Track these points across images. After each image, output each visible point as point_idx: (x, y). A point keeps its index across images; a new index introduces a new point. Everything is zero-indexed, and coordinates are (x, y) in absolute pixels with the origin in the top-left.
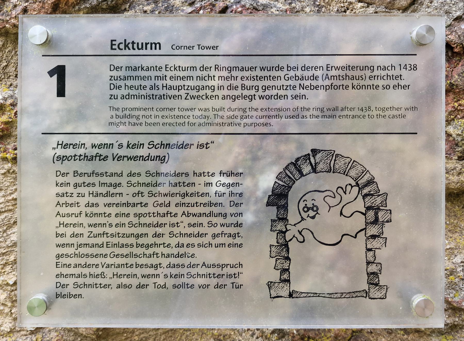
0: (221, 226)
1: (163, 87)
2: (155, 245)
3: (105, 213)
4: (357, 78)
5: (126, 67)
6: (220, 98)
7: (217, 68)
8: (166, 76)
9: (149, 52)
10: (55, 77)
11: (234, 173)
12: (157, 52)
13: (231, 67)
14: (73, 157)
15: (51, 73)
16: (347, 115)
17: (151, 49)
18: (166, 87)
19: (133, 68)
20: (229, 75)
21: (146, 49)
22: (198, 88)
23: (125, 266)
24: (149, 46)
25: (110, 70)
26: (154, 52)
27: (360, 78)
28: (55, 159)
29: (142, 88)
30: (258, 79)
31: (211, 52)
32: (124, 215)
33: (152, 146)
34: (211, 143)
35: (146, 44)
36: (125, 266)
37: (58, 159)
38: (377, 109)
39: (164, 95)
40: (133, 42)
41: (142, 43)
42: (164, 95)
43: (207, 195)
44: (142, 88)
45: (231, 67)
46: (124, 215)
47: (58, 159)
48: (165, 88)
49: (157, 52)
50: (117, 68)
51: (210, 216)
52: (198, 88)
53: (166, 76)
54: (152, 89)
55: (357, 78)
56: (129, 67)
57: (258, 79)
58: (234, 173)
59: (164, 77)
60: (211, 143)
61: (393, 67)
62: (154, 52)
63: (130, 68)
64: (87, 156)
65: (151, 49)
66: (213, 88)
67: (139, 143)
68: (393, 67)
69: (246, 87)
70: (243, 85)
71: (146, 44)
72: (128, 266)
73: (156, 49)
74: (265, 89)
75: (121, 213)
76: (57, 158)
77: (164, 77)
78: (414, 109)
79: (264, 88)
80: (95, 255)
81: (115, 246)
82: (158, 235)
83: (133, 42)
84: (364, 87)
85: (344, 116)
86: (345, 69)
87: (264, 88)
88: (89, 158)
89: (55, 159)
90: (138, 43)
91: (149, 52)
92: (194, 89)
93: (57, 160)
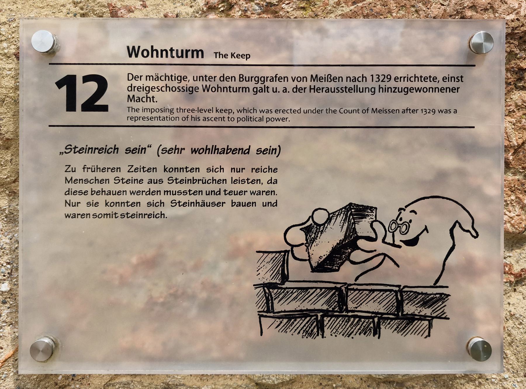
0: (131, 194)
1: (311, 89)
2: (102, 192)
3: (127, 202)
4: (333, 90)
5: (147, 76)
6: (401, 112)
7: (242, 78)
8: (268, 88)
9: (189, 60)
10: (64, 88)
11: (271, 169)
12: (200, 60)
13: (264, 77)
14: (73, 150)
15: (59, 84)
16: (421, 77)
17: (193, 57)
18: (314, 89)
19: (154, 77)
20: (263, 86)
21: (187, 57)
22: (406, 90)
23: (126, 204)
24: (190, 53)
25: (128, 80)
26: (196, 60)
27: (336, 91)
28: (160, 151)
29: (423, 80)
30: (347, 91)
31: (243, 61)
32: (136, 181)
33: (70, 150)
34: (148, 147)
35: (187, 51)
36: (126, 204)
37: (164, 152)
38: (230, 119)
39: (167, 117)
40: (172, 48)
41: (182, 51)
42: (167, 117)
43: (259, 181)
44: (423, 80)
45: (264, 77)
46: (136, 181)
47: (164, 152)
48: (312, 91)
49: (200, 60)
50: (135, 78)
51: (69, 194)
52: (406, 90)
53: (268, 88)
54: (273, 81)
55: (333, 90)
56: (150, 77)
57: (347, 91)
58: (271, 169)
59: (266, 89)
60: (148, 147)
61: (364, 78)
62: (196, 60)
63: (151, 77)
64: (218, 149)
65: (193, 57)
66: (373, 90)
67: (88, 147)
68: (364, 78)
69: (244, 78)
70: (241, 76)
71: (252, 77)
72: (129, 204)
73: (198, 57)
74: (407, 92)
75: (133, 179)
76: (162, 150)
77: (266, 89)
78: (179, 111)
79: (255, 90)
80: (216, 203)
81: (193, 204)
82: (152, 192)
83: (172, 48)
84: (431, 89)
85: (156, 118)
86: (447, 80)
87: (255, 90)
88: (220, 151)
89: (160, 151)
90: (177, 51)
91: (189, 60)
92: (402, 92)
93: (162, 153)
